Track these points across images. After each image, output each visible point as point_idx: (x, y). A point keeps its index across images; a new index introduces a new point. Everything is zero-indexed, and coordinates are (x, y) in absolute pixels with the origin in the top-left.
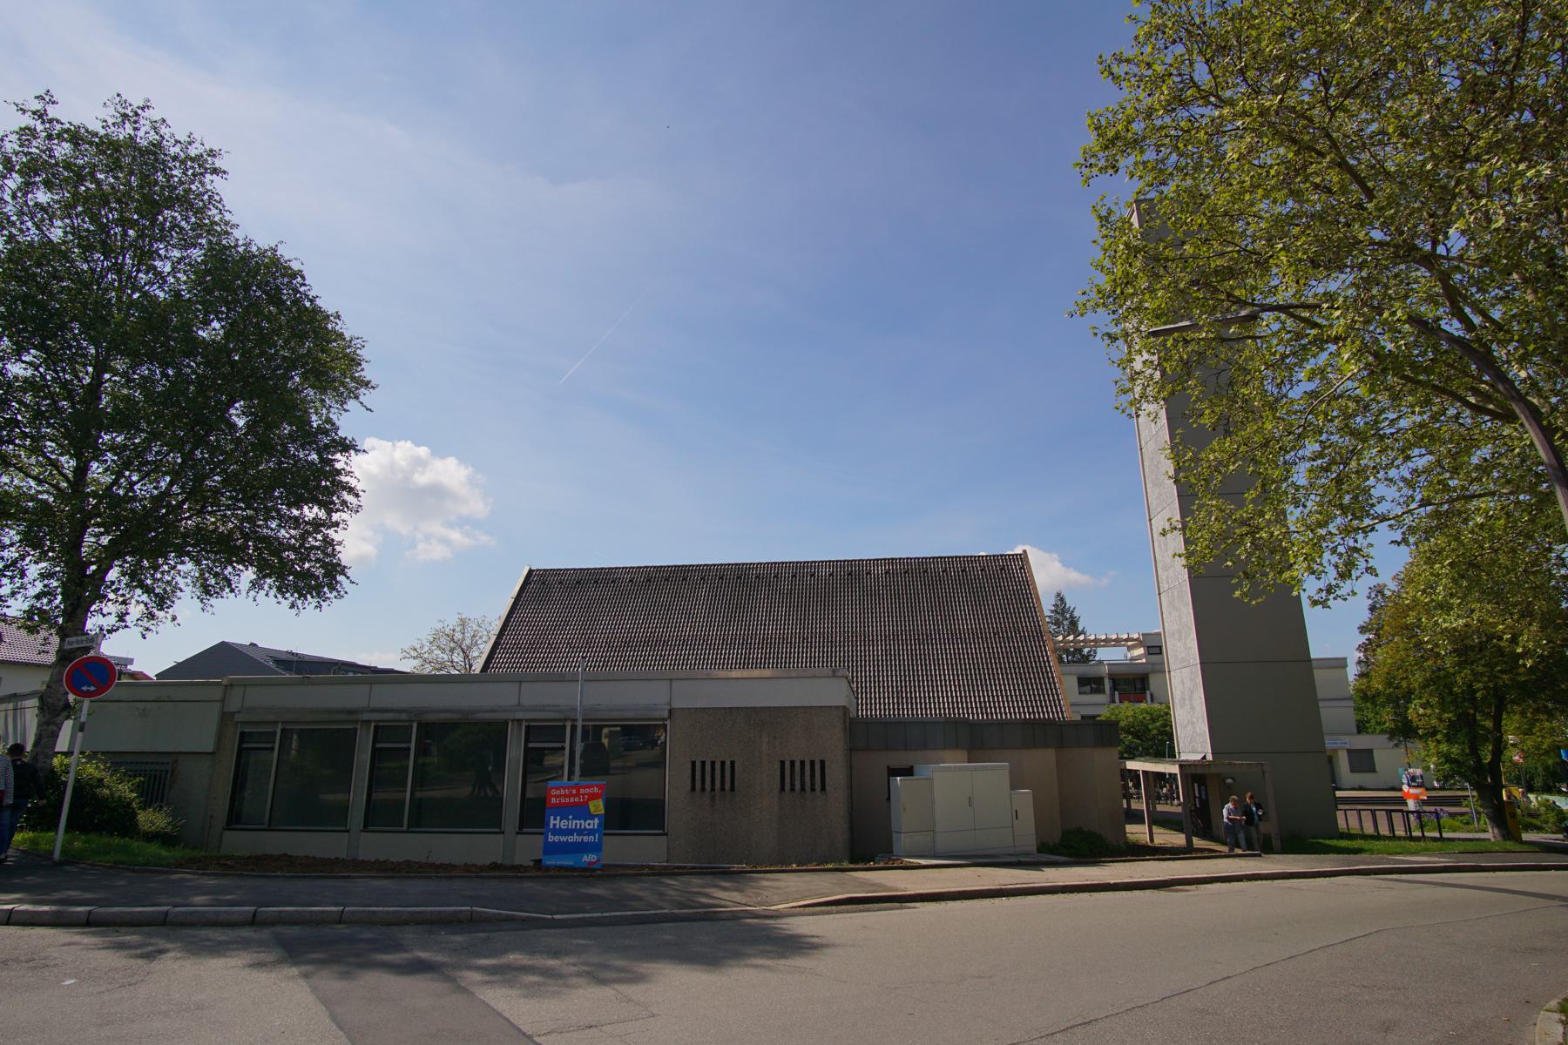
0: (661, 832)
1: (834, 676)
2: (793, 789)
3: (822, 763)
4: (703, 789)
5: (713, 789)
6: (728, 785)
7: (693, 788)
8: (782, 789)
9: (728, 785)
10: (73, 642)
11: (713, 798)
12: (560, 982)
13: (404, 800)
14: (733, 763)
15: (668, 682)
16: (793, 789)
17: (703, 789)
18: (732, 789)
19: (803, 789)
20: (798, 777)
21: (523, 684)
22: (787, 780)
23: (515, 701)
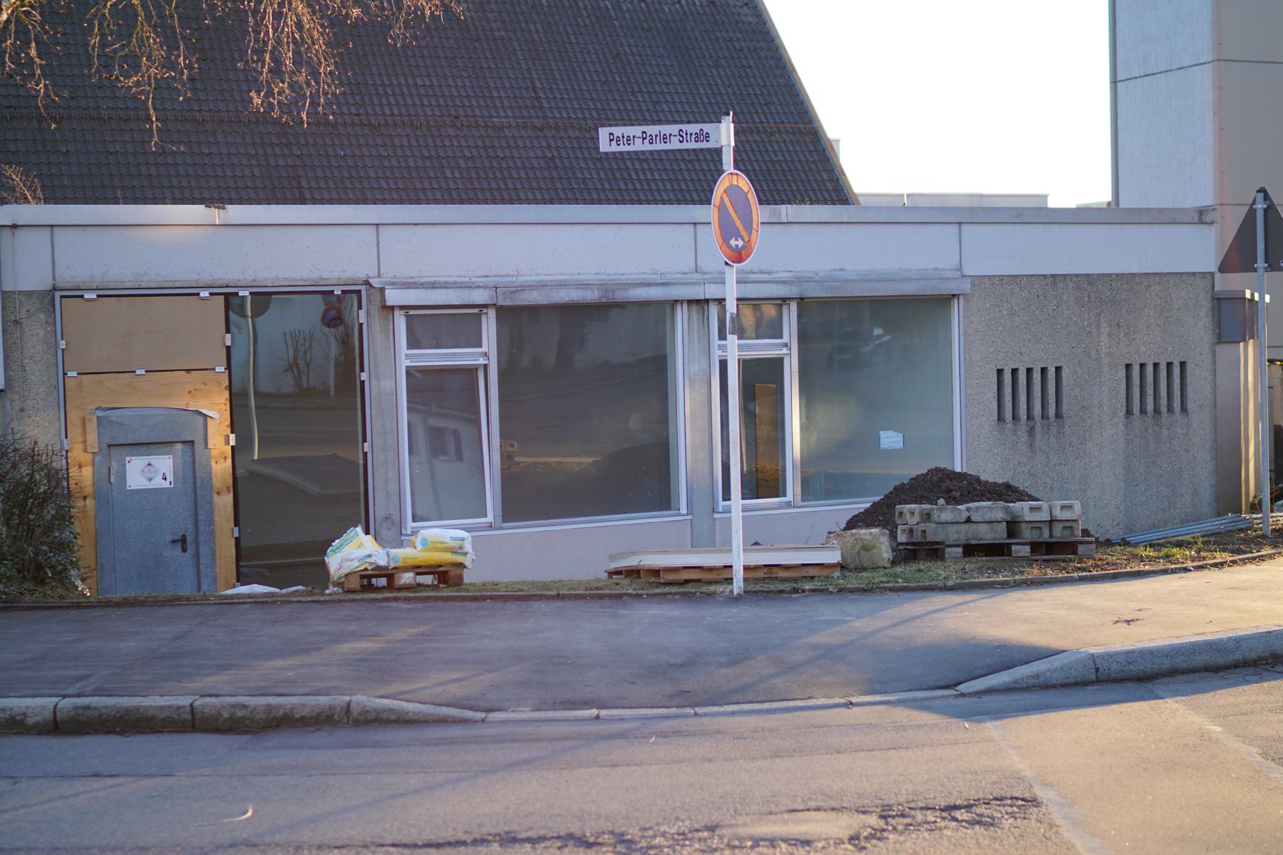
0: (412, 312)
1: (1201, 222)
2: (1143, 411)
3: (1183, 364)
4: (1015, 417)
5: (1030, 417)
6: (1052, 411)
7: (1000, 418)
8: (1129, 412)
9: (1052, 411)
10: (758, 314)
11: (1031, 431)
12: (456, 588)
13: (359, 493)
14: (1058, 369)
15: (374, 228)
16: (1143, 411)
17: (1015, 417)
18: (1058, 415)
19: (1157, 411)
20: (1150, 390)
21: (380, 227)
22: (1136, 396)
23: (687, 264)
